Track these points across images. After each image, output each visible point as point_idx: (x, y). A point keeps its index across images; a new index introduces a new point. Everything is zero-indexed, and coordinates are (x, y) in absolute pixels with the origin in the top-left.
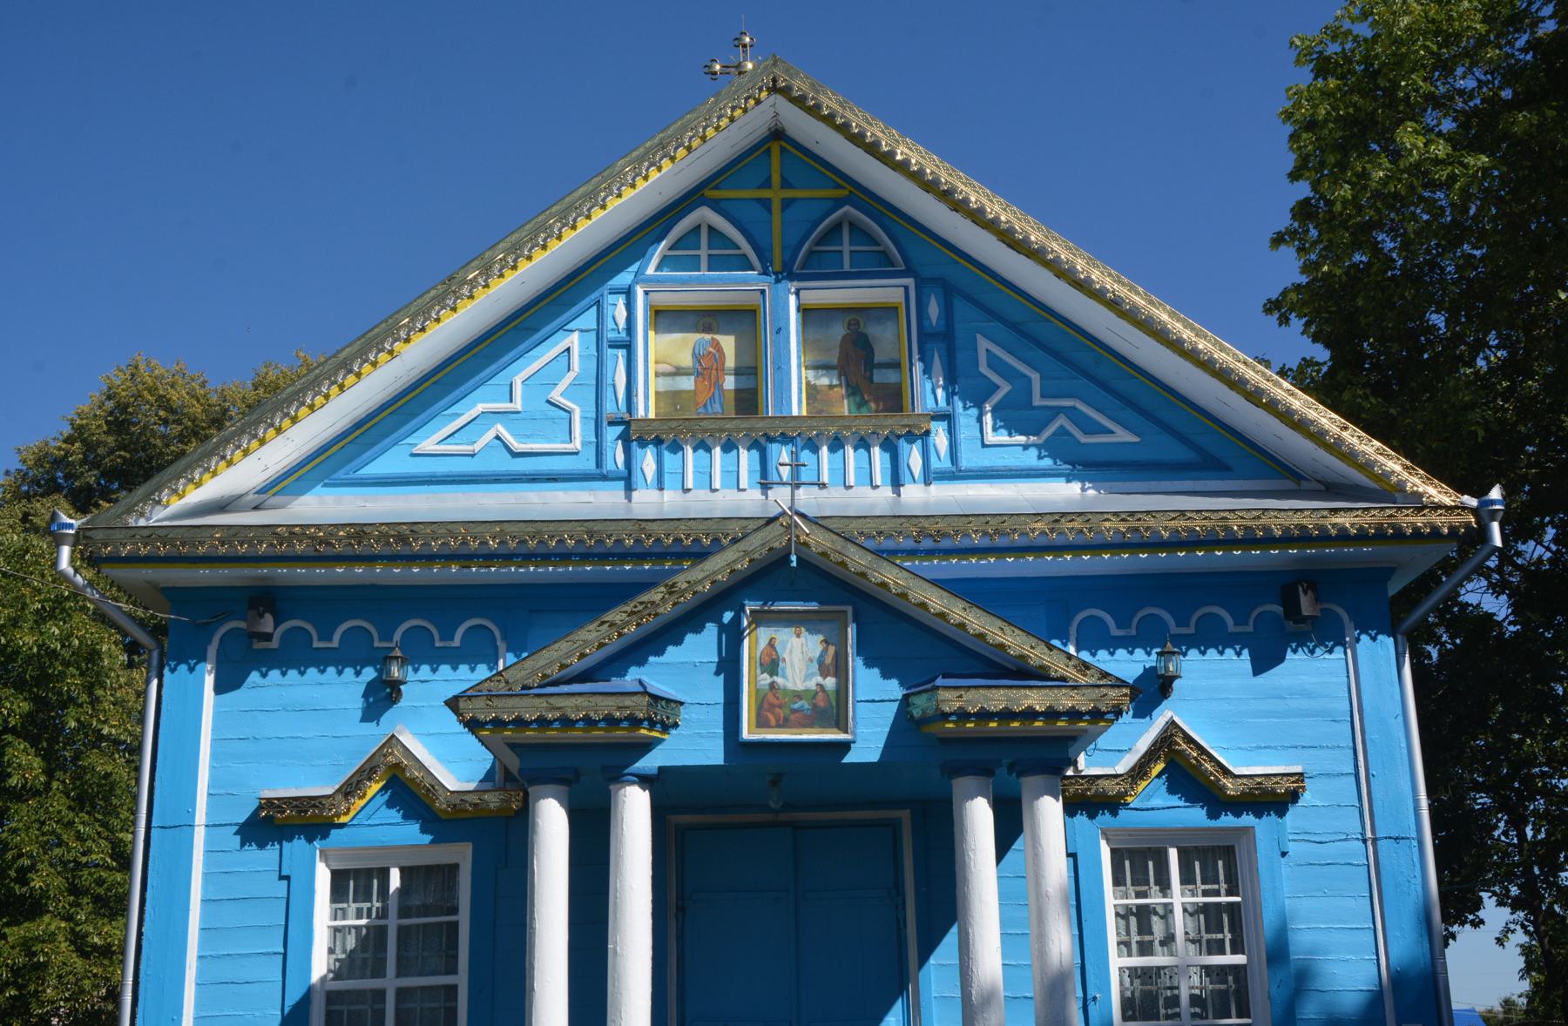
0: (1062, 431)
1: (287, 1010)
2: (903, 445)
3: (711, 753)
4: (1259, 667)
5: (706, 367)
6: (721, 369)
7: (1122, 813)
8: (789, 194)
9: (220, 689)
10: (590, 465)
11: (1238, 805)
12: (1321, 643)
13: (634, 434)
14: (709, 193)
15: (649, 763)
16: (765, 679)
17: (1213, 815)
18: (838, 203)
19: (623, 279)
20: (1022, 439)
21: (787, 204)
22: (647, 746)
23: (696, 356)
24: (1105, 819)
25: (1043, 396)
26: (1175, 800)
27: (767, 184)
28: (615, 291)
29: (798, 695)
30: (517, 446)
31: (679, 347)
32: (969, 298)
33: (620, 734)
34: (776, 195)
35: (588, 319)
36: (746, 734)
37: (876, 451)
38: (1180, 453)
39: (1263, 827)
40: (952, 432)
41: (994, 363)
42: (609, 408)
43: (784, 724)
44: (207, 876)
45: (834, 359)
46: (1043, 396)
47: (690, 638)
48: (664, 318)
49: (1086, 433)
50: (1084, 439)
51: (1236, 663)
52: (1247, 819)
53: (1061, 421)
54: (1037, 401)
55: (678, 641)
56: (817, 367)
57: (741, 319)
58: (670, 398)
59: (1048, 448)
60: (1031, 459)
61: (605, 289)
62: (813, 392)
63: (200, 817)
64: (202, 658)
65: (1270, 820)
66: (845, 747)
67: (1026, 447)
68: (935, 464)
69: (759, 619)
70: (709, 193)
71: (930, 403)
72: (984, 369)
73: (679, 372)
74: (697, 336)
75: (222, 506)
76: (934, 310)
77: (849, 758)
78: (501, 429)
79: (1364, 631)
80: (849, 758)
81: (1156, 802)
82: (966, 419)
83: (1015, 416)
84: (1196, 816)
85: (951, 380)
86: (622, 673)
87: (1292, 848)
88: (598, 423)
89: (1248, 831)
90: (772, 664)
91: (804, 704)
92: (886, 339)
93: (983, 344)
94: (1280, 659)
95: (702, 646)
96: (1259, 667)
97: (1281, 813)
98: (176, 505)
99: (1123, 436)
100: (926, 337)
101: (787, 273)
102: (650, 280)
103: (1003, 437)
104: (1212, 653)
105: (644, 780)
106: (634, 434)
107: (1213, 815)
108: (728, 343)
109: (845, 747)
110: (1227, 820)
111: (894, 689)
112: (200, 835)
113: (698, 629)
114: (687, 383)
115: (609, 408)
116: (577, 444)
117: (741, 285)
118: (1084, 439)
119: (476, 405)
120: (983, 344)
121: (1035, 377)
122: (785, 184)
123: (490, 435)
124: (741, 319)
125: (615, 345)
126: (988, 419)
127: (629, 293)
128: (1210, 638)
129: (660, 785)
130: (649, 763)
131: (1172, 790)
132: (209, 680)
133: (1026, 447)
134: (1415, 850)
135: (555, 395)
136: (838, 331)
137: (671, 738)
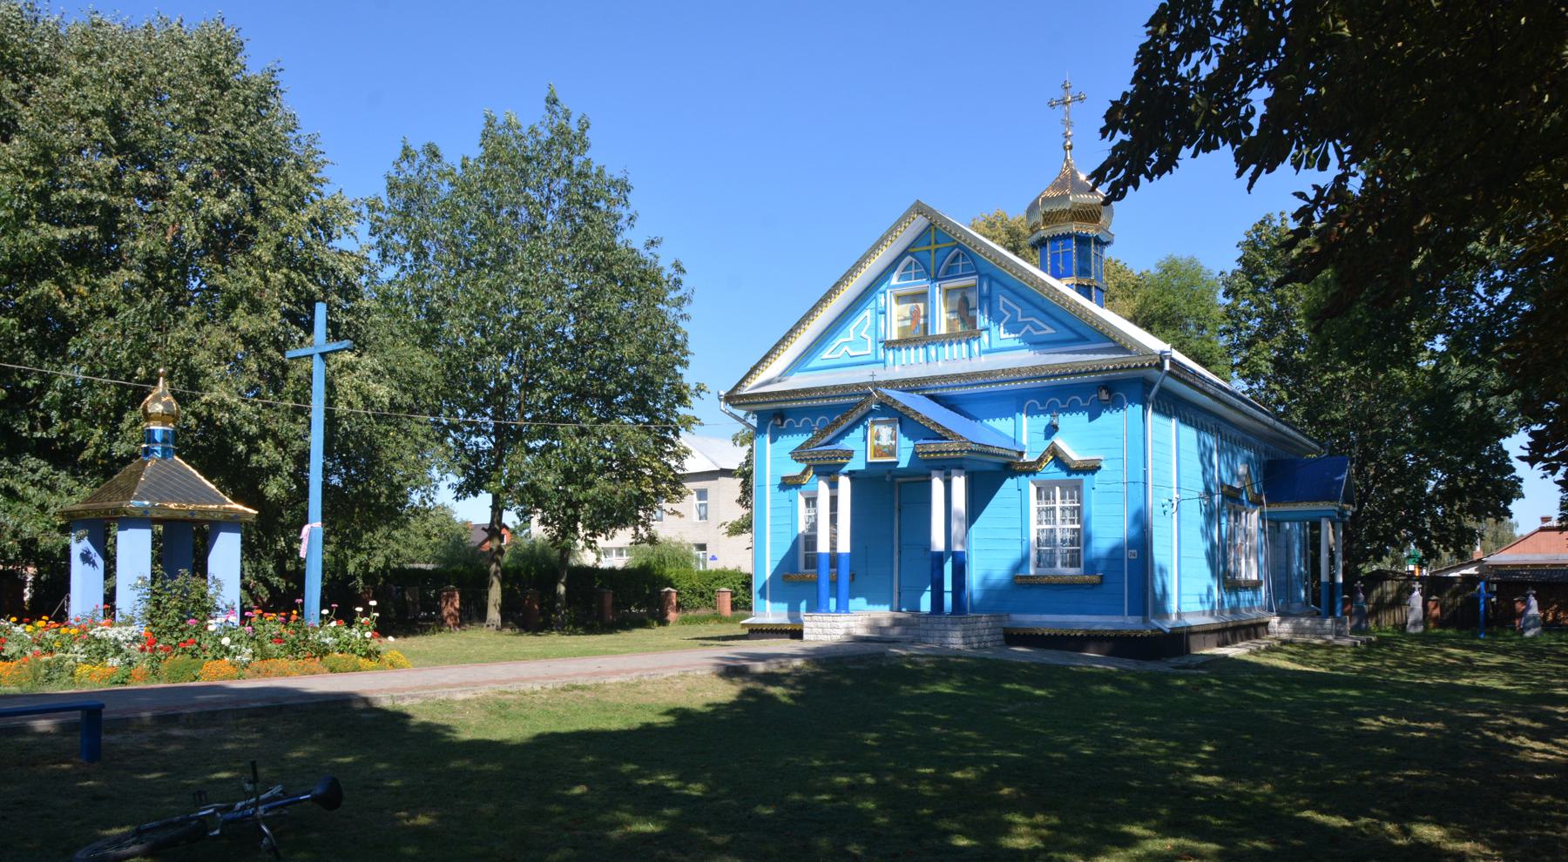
0: (1028, 331)
1: (1438, 575)
2: (972, 341)
3: (862, 467)
4: (1091, 419)
5: (914, 315)
6: (919, 316)
7: (1038, 475)
8: (937, 246)
9: (772, 442)
10: (873, 358)
11: (1078, 471)
12: (1115, 408)
13: (889, 345)
14: (911, 250)
15: (846, 469)
16: (876, 442)
17: (1069, 475)
18: (954, 248)
19: (883, 288)
20: (1013, 335)
21: (936, 250)
22: (844, 465)
23: (911, 313)
24: (1032, 476)
25: (1022, 317)
26: (1057, 470)
27: (930, 244)
28: (881, 293)
29: (885, 447)
30: (852, 354)
31: (906, 309)
32: (998, 281)
33: (833, 462)
34: (933, 247)
35: (872, 305)
36: (869, 460)
37: (964, 344)
38: (1072, 336)
39: (1086, 479)
40: (989, 335)
41: (1006, 307)
42: (879, 337)
43: (881, 456)
44: (771, 500)
45: (956, 308)
46: (1022, 317)
47: (856, 430)
48: (901, 299)
49: (1036, 330)
50: (1035, 333)
51: (1081, 418)
52: (1081, 476)
53: (1028, 327)
54: (1020, 320)
55: (853, 431)
56: (951, 312)
57: (921, 296)
58: (903, 329)
59: (1022, 338)
60: (1016, 343)
61: (877, 292)
62: (949, 322)
63: (768, 483)
64: (765, 433)
65: (1089, 476)
66: (897, 463)
67: (1015, 339)
68: (983, 348)
69: (874, 423)
70: (911, 250)
71: (982, 325)
72: (1001, 309)
73: (906, 319)
74: (910, 305)
75: (769, 382)
76: (985, 287)
77: (899, 466)
78: (846, 348)
79: (1130, 403)
80: (899, 466)
81: (1050, 470)
82: (994, 329)
83: (1012, 327)
84: (1063, 475)
85: (990, 315)
86: (838, 442)
87: (1096, 486)
88: (877, 341)
89: (1081, 480)
90: (878, 437)
91: (886, 450)
92: (973, 298)
93: (1002, 299)
94: (1099, 415)
95: (859, 432)
96: (1091, 419)
97: (1093, 474)
98: (750, 386)
99: (1050, 331)
100: (981, 298)
101: (936, 279)
102: (894, 287)
103: (1007, 335)
104: (1074, 414)
105: (845, 474)
106: (889, 345)
107: (1069, 475)
108: (921, 306)
109: (897, 463)
110: (1074, 477)
111: (911, 444)
112: (768, 488)
113: (858, 427)
114: (908, 323)
115: (879, 337)
116: (869, 352)
117: (921, 284)
118: (1035, 333)
119: (840, 340)
120: (1002, 299)
121: (1019, 310)
122: (936, 243)
123: (843, 351)
124: (921, 296)
125: (881, 313)
126: (1002, 329)
127: (884, 292)
128: (1073, 409)
129: (851, 474)
130: (846, 469)
131: (1056, 466)
132: (768, 440)
133: (1015, 339)
134: (1141, 489)
135: (863, 334)
136: (958, 297)
137: (851, 461)
